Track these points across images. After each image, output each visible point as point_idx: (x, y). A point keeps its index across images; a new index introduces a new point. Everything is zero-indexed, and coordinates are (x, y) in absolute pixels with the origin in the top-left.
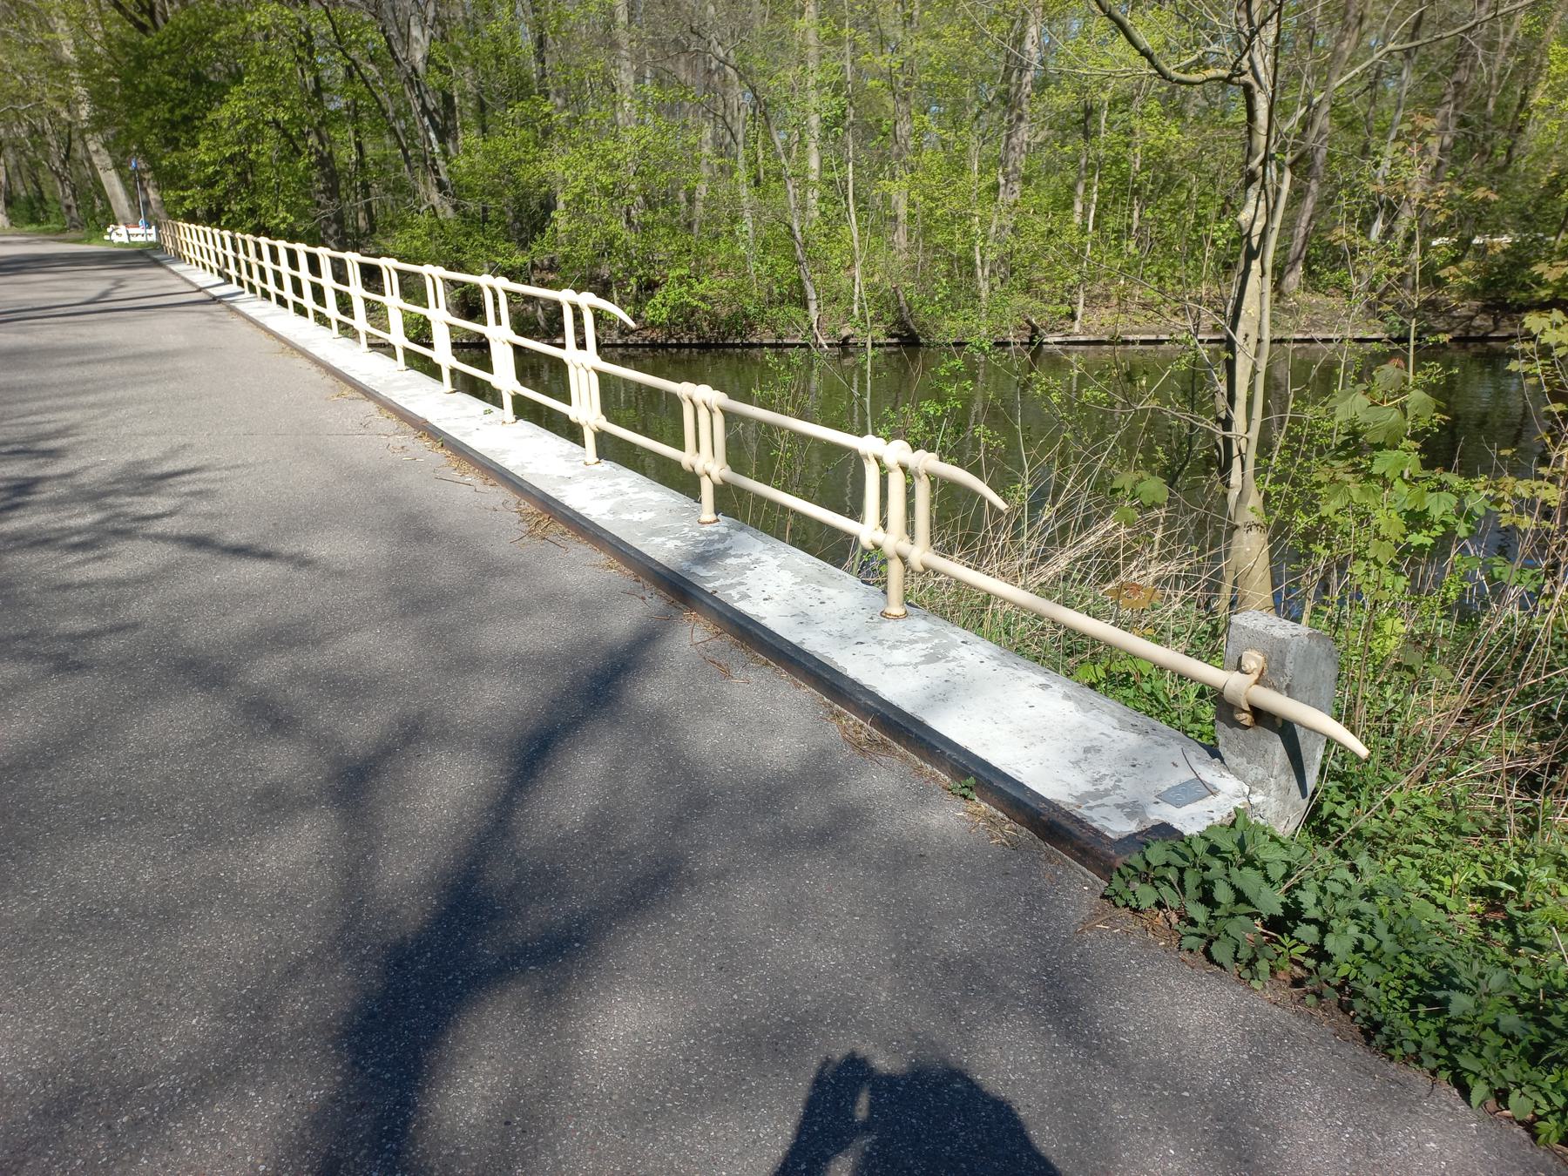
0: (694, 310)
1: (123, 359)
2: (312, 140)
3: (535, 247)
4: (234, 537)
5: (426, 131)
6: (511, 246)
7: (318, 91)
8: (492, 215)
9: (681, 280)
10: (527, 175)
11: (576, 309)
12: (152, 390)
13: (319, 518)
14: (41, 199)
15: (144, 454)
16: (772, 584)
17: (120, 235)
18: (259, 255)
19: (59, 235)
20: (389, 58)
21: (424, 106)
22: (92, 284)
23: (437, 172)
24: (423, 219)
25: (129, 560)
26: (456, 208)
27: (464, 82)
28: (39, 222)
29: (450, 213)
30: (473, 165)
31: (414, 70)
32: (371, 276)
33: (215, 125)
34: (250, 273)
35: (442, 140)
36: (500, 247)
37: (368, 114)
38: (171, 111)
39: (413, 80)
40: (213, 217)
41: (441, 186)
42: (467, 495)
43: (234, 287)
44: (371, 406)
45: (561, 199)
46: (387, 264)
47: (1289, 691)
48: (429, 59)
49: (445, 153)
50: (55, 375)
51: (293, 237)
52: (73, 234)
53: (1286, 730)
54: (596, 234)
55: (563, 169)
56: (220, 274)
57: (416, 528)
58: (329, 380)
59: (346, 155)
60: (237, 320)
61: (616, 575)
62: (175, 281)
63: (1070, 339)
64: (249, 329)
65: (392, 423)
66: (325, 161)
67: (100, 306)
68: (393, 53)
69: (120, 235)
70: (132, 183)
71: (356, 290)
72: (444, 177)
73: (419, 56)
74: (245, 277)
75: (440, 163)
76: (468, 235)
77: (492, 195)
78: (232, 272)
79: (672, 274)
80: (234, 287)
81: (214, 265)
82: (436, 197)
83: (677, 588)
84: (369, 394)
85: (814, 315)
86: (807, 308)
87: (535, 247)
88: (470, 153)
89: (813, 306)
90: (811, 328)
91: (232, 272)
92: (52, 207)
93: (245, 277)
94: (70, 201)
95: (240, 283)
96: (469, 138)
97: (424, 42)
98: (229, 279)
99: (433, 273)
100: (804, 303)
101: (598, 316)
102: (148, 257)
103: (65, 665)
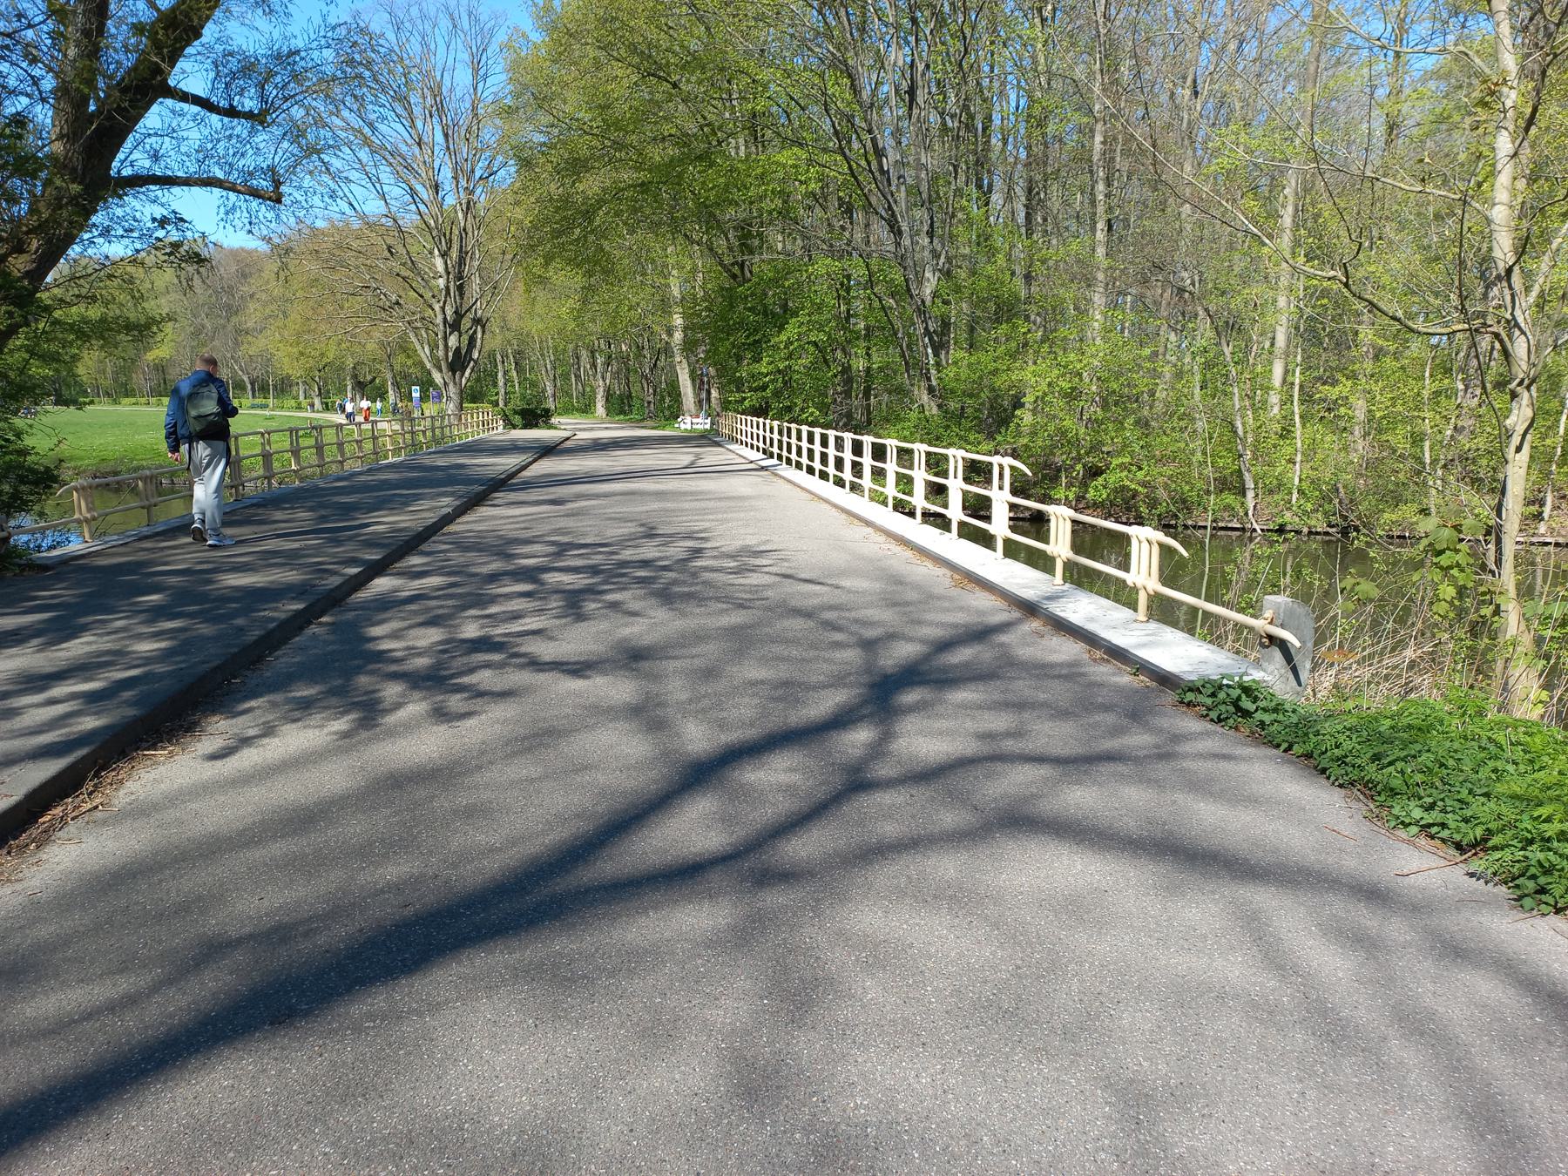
0: (1135, 494)
1: (720, 499)
2: (839, 354)
3: (999, 438)
4: (803, 576)
5: (925, 347)
6: (980, 437)
7: (849, 316)
8: (969, 411)
9: (1122, 467)
10: (1000, 382)
11: (1001, 466)
12: (742, 515)
13: (843, 573)
14: (630, 396)
15: (748, 542)
16: (1083, 608)
17: (686, 424)
18: (799, 439)
19: (639, 423)
20: (904, 292)
21: (926, 329)
22: (683, 456)
23: (929, 379)
24: (914, 415)
25: (754, 579)
26: (940, 406)
27: (960, 311)
28: (625, 413)
29: (935, 410)
30: (958, 374)
31: (923, 302)
32: (879, 453)
33: (776, 348)
34: (789, 451)
35: (936, 355)
36: (972, 438)
37: (882, 332)
38: (747, 337)
39: (922, 310)
40: (760, 411)
41: (931, 390)
42: (925, 571)
43: (775, 461)
44: (870, 530)
45: (1028, 399)
46: (892, 443)
47: (1282, 626)
48: (935, 295)
49: (938, 364)
50: (686, 505)
51: (811, 424)
52: (649, 423)
53: (1282, 645)
54: (1051, 428)
55: (1033, 376)
56: (765, 452)
57: (898, 580)
58: (844, 516)
59: (859, 364)
60: (781, 481)
61: (1000, 603)
62: (732, 456)
63: (1535, 540)
64: (790, 486)
65: (882, 538)
66: (846, 369)
67: (690, 470)
68: (909, 290)
69: (686, 424)
70: (699, 381)
71: (867, 461)
72: (934, 383)
73: (928, 291)
74: (785, 453)
75: (933, 371)
76: (947, 427)
77: (971, 396)
78: (775, 450)
79: (1115, 462)
80: (775, 461)
81: (761, 445)
82: (925, 398)
83: (1030, 609)
84: (868, 523)
85: (1250, 503)
86: (1244, 495)
87: (999, 438)
88: (958, 364)
89: (1250, 494)
90: (1246, 514)
91: (775, 450)
92: (636, 403)
93: (785, 453)
94: (651, 398)
95: (780, 457)
96: (955, 354)
97: (934, 281)
98: (771, 456)
99: (920, 448)
100: (1242, 492)
101: (1012, 468)
102: (708, 439)
103: (741, 606)
